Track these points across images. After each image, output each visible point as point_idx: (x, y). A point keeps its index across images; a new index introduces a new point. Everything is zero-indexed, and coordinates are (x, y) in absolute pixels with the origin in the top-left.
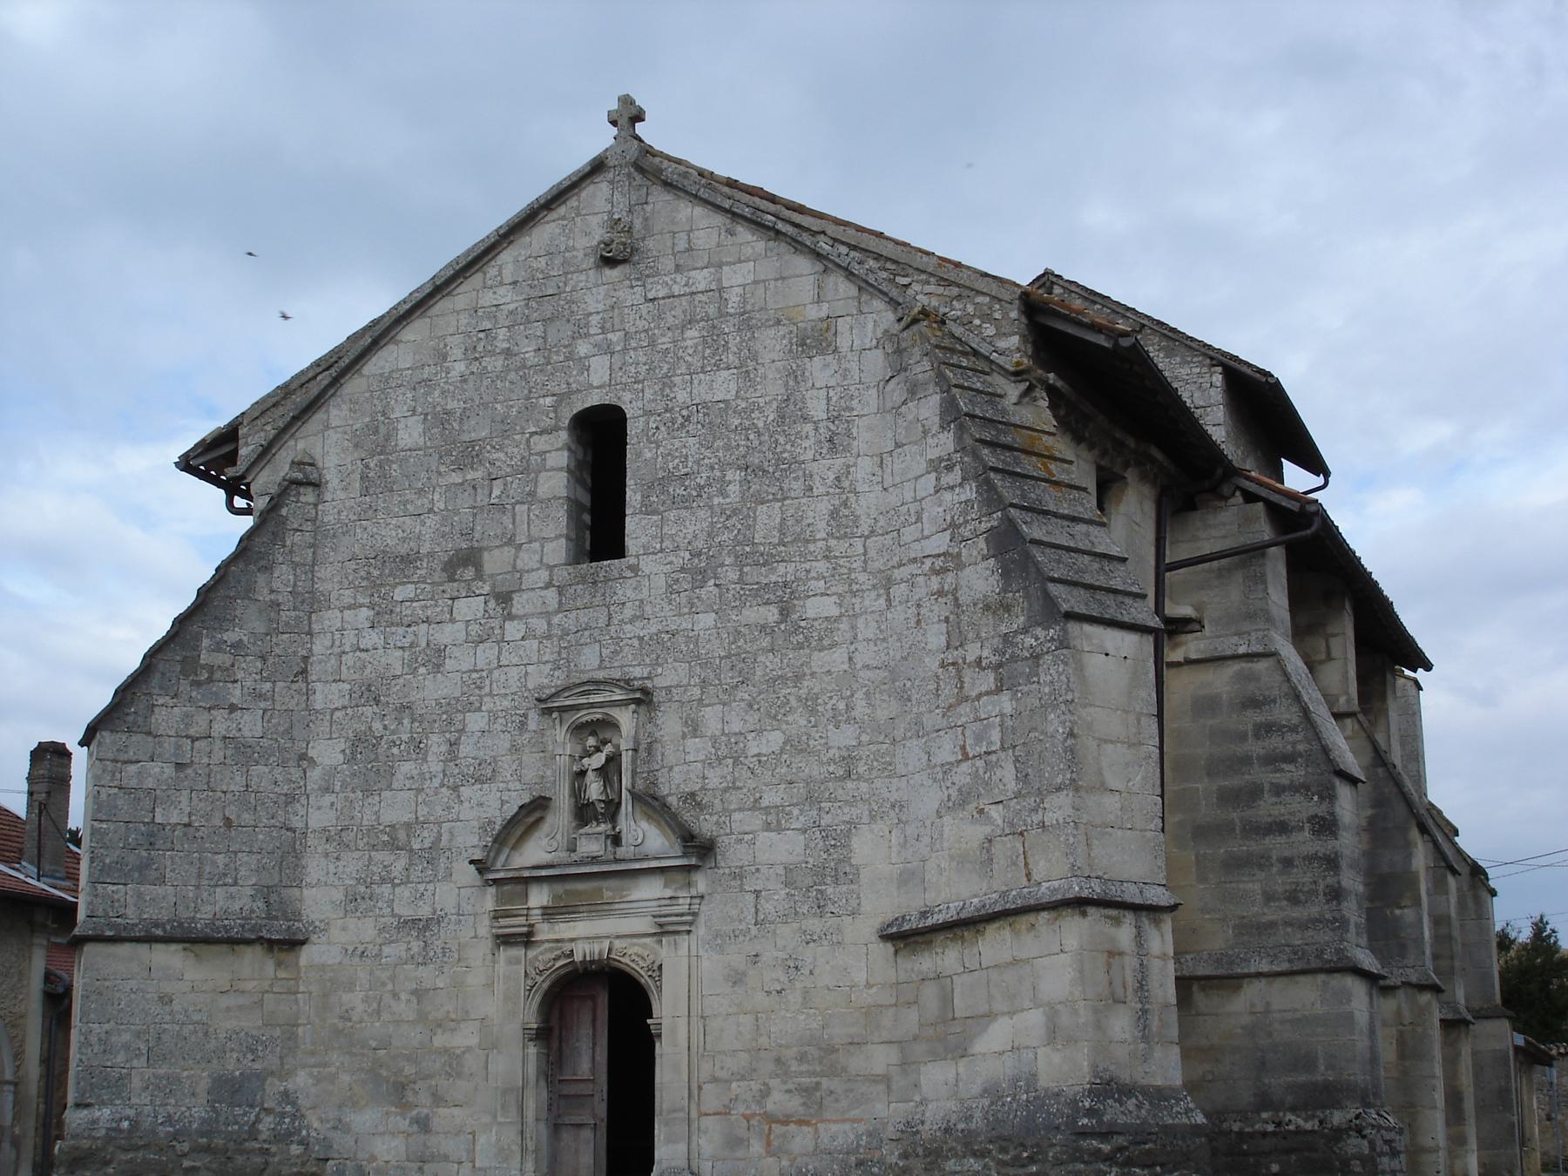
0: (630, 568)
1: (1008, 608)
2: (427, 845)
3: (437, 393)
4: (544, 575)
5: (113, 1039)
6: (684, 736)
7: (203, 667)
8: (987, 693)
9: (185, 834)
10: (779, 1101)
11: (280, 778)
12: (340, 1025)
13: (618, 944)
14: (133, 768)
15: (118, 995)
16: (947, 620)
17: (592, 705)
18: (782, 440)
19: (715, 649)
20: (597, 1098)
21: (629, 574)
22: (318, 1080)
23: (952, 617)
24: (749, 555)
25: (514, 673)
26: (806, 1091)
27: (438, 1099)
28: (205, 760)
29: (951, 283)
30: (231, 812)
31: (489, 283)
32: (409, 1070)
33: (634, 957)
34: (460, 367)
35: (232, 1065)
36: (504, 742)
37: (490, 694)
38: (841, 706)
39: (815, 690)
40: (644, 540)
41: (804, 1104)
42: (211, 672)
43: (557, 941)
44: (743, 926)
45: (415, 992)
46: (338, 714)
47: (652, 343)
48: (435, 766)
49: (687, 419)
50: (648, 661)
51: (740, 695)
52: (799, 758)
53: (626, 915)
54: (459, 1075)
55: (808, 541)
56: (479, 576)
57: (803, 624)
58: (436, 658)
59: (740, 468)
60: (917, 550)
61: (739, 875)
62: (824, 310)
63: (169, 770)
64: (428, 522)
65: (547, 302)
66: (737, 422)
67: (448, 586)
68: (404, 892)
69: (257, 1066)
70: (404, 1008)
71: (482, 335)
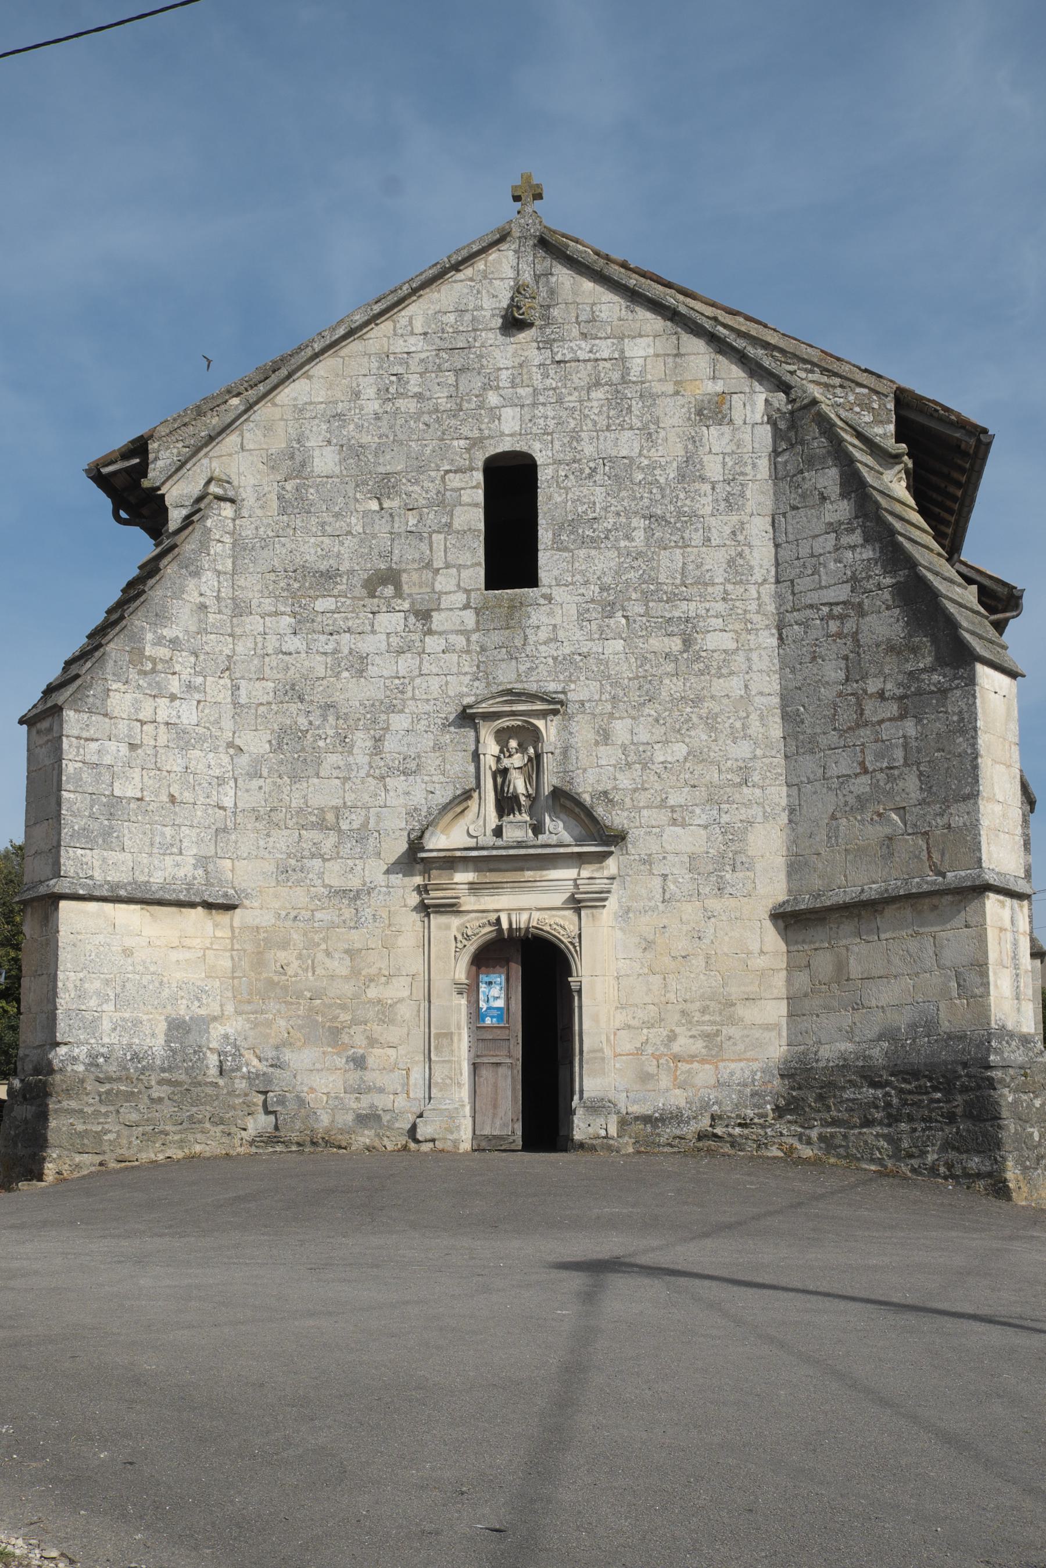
0: (544, 596)
1: (914, 650)
2: (355, 826)
3: (352, 427)
4: (461, 598)
5: (86, 985)
6: (597, 743)
7: (149, 658)
8: (890, 719)
9: (139, 807)
10: (683, 1044)
11: (213, 763)
12: (276, 979)
13: (536, 915)
14: (94, 746)
15: (89, 947)
16: (846, 658)
17: (513, 714)
18: (682, 496)
19: (625, 670)
20: (512, 1041)
21: (542, 601)
22: (256, 1025)
23: (851, 656)
24: (651, 591)
25: (435, 683)
26: (707, 1037)
27: (372, 1042)
28: (152, 743)
29: (836, 375)
30: (175, 790)
31: (400, 331)
32: (345, 1017)
33: (559, 924)
34: (374, 406)
35: (183, 1010)
36: (428, 741)
37: (413, 698)
38: (738, 725)
39: (715, 711)
40: (556, 572)
41: (706, 1047)
42: (155, 664)
43: (483, 911)
44: (652, 904)
45: (347, 952)
46: (262, 709)
47: (560, 401)
48: (360, 758)
49: (594, 470)
50: (561, 677)
51: (646, 711)
52: (701, 766)
53: (546, 891)
54: (392, 1021)
55: (706, 584)
56: (399, 593)
57: (704, 654)
58: (360, 665)
59: (644, 517)
60: (813, 598)
61: (648, 861)
62: (719, 387)
63: (124, 749)
64: (347, 543)
65: (454, 354)
66: (640, 477)
67: (367, 601)
68: (335, 866)
69: (202, 1012)
70: (340, 966)
71: (393, 378)
